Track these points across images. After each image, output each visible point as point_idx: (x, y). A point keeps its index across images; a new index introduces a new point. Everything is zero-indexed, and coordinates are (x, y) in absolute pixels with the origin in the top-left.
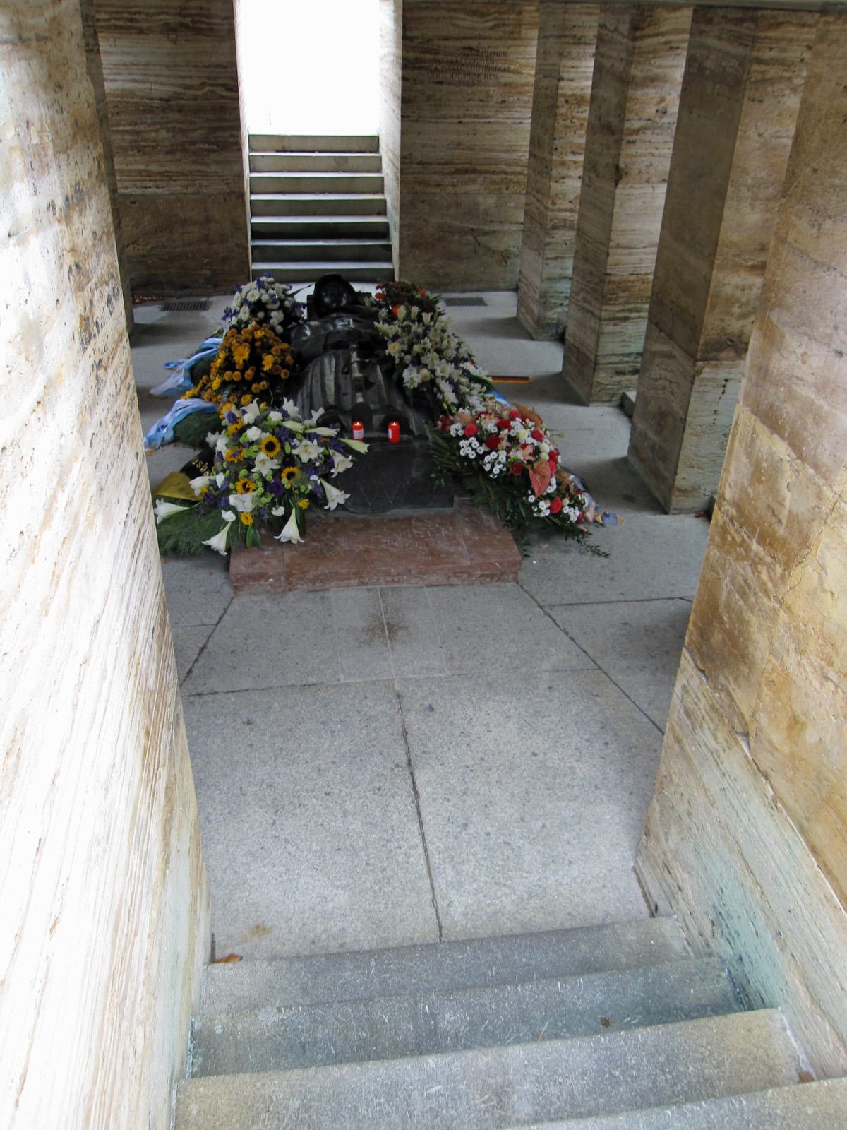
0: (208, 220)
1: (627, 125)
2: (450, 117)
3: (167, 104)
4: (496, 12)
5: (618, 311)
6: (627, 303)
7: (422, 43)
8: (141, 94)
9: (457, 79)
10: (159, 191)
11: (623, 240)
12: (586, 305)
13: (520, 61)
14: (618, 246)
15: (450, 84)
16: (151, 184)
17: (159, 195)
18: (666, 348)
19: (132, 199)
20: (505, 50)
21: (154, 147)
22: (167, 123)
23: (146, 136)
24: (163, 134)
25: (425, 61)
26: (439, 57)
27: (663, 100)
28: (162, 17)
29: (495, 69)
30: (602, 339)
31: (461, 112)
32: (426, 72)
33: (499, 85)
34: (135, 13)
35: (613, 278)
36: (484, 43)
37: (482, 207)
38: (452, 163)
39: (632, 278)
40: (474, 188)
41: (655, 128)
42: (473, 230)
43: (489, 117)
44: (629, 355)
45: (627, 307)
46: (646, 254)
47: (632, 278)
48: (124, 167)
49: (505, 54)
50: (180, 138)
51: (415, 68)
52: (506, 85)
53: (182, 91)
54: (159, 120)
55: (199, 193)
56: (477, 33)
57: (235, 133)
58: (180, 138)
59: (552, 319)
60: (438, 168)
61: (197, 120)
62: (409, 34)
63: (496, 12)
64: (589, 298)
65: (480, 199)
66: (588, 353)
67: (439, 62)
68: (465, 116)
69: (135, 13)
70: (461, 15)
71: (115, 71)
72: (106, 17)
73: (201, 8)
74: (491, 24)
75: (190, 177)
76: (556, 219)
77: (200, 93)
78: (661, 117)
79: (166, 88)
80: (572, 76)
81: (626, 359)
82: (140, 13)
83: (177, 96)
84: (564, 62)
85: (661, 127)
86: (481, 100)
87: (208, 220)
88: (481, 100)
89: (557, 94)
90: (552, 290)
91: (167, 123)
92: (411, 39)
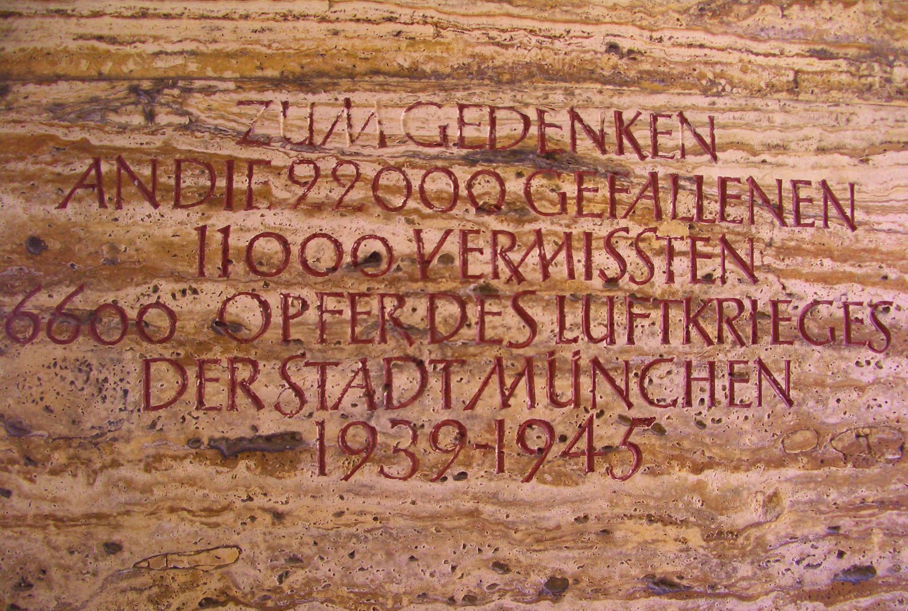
9: (430, 410)
20: (840, 171)
25: (118, 267)
32: (130, 356)
49: (838, 206)
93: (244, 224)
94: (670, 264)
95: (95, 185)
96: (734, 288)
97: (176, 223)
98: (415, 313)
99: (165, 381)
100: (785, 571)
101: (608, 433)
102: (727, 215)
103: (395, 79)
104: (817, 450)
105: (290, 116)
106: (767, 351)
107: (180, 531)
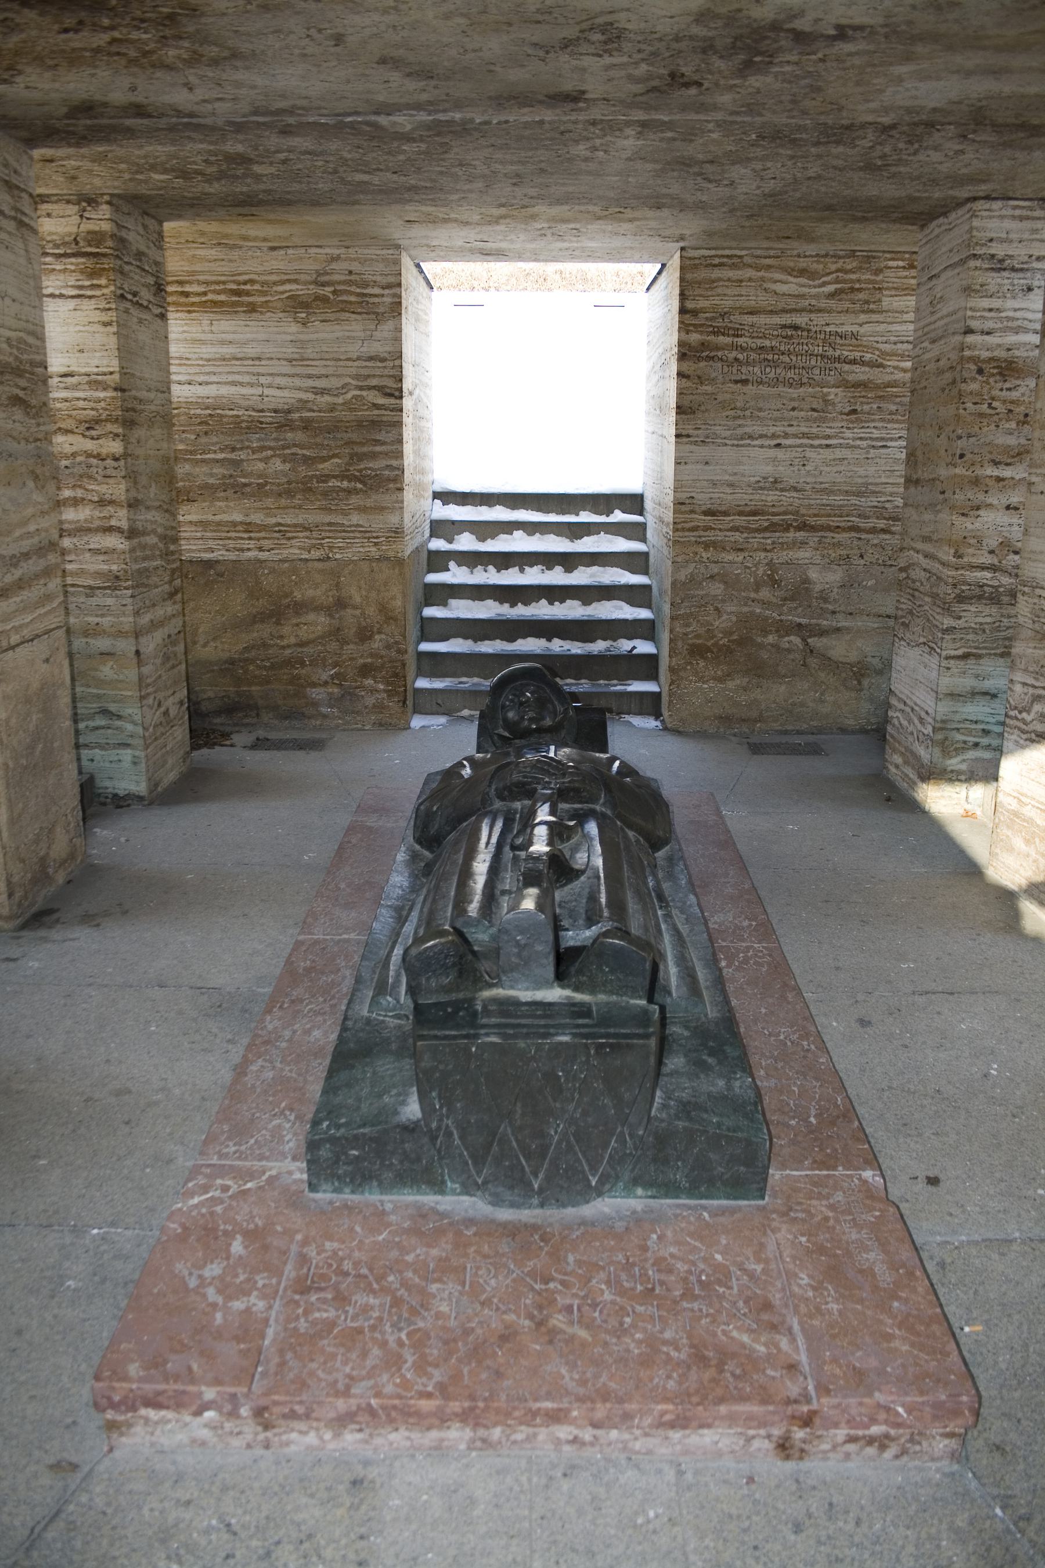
0: (341, 604)
2: (761, 436)
4: (837, 271)
7: (712, 319)
9: (772, 375)
16: (252, 544)
20: (855, 329)
22: (284, 448)
24: (277, 465)
26: (741, 341)
28: (287, 287)
32: (720, 365)
34: (245, 283)
36: (819, 319)
37: (818, 588)
40: (803, 555)
42: (800, 625)
43: (829, 437)
49: (854, 336)
50: (303, 471)
51: (699, 359)
52: (857, 385)
53: (310, 396)
54: (272, 444)
57: (394, 463)
58: (303, 471)
60: (740, 521)
62: (690, 305)
63: (837, 271)
65: (813, 574)
67: (743, 349)
68: (786, 435)
69: (245, 283)
70: (778, 276)
71: (207, 369)
72: (201, 289)
73: (350, 272)
75: (315, 534)
76: (965, 583)
77: (340, 400)
80: (990, 325)
82: (252, 282)
88: (814, 410)
90: (957, 717)
92: (695, 313)
93: (741, 341)
94: (137, 643)
95: (714, 333)
96: (831, 352)
97: (728, 340)
98: (770, 357)
99: (726, 369)
100: (839, 407)
101: (805, 380)
102: (831, 339)
104: (845, 384)
105: (749, 319)
106: (837, 365)
107: (728, 396)
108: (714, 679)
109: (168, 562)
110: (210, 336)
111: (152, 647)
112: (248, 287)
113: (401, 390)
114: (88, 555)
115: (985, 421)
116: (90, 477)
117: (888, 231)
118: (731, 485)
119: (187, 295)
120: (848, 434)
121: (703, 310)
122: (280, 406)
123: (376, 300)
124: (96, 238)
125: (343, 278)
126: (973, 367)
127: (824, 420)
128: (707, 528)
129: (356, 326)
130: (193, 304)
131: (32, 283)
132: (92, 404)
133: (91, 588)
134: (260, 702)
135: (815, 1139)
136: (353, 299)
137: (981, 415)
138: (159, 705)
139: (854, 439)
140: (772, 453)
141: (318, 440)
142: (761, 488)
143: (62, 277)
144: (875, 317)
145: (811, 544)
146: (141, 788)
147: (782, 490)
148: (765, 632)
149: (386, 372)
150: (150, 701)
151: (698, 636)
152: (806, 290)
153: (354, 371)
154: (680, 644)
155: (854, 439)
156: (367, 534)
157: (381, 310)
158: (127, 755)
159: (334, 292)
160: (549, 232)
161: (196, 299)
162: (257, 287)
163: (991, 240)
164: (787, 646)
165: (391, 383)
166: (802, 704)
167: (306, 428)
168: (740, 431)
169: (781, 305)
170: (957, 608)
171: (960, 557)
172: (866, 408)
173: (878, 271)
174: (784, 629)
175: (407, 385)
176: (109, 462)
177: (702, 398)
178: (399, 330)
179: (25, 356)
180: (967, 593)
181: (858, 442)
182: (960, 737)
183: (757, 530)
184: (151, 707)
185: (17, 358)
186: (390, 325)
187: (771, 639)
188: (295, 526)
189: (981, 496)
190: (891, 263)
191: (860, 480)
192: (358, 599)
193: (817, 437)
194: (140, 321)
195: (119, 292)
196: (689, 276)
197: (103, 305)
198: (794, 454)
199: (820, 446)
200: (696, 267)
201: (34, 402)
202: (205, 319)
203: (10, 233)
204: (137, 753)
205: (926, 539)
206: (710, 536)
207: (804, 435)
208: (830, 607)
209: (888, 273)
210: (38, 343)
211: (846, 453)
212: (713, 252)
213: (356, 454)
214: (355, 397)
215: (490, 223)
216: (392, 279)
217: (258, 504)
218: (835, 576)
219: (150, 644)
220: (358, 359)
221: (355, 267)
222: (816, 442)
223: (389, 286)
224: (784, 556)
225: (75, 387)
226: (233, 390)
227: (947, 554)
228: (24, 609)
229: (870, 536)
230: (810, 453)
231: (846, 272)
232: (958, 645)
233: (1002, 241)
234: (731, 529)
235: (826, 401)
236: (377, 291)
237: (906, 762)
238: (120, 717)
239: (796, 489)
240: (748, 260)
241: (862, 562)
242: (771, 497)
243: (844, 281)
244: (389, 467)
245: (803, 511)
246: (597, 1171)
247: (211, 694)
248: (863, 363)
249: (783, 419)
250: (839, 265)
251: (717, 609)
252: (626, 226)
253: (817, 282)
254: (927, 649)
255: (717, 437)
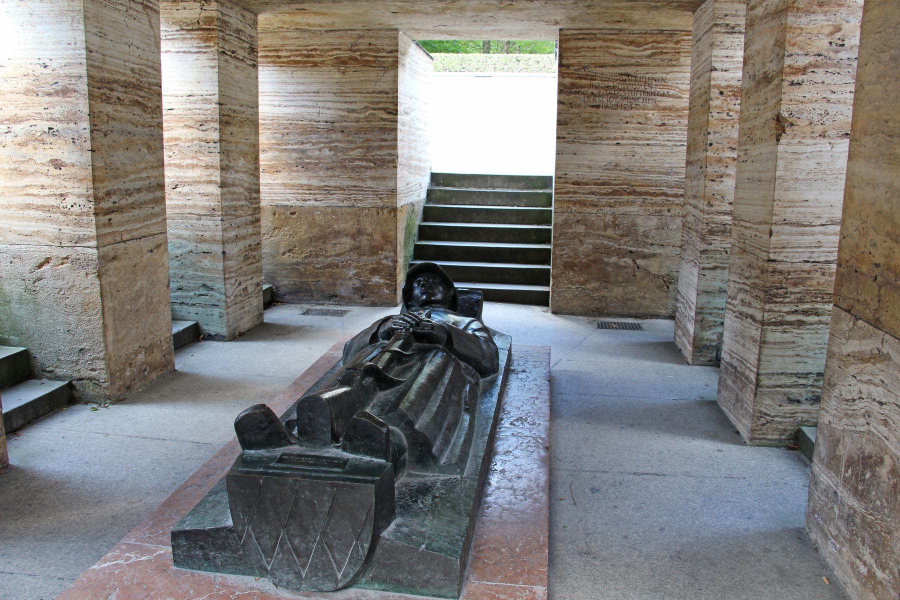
0: (360, 232)
1: (788, 61)
2: (608, 139)
3: (331, 127)
4: (653, 42)
5: (788, 313)
6: (801, 301)
7: (578, 70)
8: (310, 117)
9: (614, 103)
10: (317, 204)
11: (791, 215)
12: (745, 310)
13: (680, 86)
14: (785, 222)
15: (607, 107)
16: (311, 197)
17: (316, 208)
18: (869, 346)
19: (292, 210)
20: (664, 76)
21: (316, 164)
22: (330, 142)
23: (309, 154)
24: (327, 152)
25: (582, 87)
26: (595, 82)
27: (838, 29)
28: (335, 52)
29: (654, 94)
30: (766, 351)
31: (618, 135)
32: (582, 96)
33: (657, 108)
34: (312, 50)
35: (779, 267)
36: (641, 71)
37: (642, 229)
38: (609, 184)
39: (807, 267)
40: (634, 209)
41: (828, 66)
42: (631, 252)
43: (648, 139)
44: (806, 375)
45: (802, 307)
46: (824, 234)
47: (807, 267)
48: (289, 182)
49: (663, 80)
50: (341, 156)
51: (570, 93)
52: (665, 109)
53: (346, 114)
54: (324, 140)
55: (354, 206)
56: (633, 61)
57: (392, 152)
58: (341, 156)
59: (712, 341)
60: (595, 188)
61: (357, 140)
62: (565, 62)
63: (653, 42)
64: (748, 298)
65: (639, 221)
66: (747, 372)
67: (596, 87)
68: (623, 138)
69: (312, 50)
70: (617, 45)
71: (290, 98)
72: (288, 54)
73: (370, 44)
74: (649, 52)
75: (346, 192)
76: (713, 223)
77: (362, 116)
78: (837, 52)
79: (332, 112)
80: (725, 66)
81: (802, 381)
82: (315, 50)
83: (343, 119)
84: (715, 52)
85: (838, 64)
86: (640, 123)
87: (360, 232)
88: (640, 123)
89: (710, 86)
90: (710, 306)
91: (330, 142)
92: (568, 66)
93: (595, 82)
95: (579, 78)
96: (649, 90)
97: (588, 82)
99: (586, 99)
100: (654, 122)
103: (659, 198)
105: (599, 70)
107: (587, 115)
108: (579, 282)
109: (252, 203)
110: (292, 80)
111: (235, 250)
112: (313, 53)
113: (397, 110)
114: (198, 196)
115: (725, 124)
116: (201, 152)
117: (676, 16)
118: (589, 167)
119: (280, 57)
120: (660, 137)
121: (573, 65)
122: (329, 119)
123: (382, 59)
124: (209, 20)
125: (365, 47)
126: (717, 91)
127: (646, 129)
128: (575, 193)
129: (372, 74)
130: (283, 62)
131: (153, 39)
132: (203, 112)
133: (199, 215)
134: (313, 288)
135: (513, 562)
136: (371, 59)
137: (722, 120)
138: (240, 284)
139: (664, 141)
140: (614, 148)
141: (350, 138)
142: (608, 169)
143: (190, 42)
144: (676, 69)
145: (638, 203)
146: (224, 331)
147: (621, 170)
148: (609, 254)
149: (389, 100)
150: (233, 281)
151: (570, 257)
152: (634, 53)
153: (371, 100)
154: (558, 261)
155: (664, 141)
156: (376, 193)
157: (386, 65)
158: (216, 311)
159: (361, 55)
160: (477, 19)
161: (285, 60)
162: (318, 52)
163: (726, 15)
164: (623, 264)
165: (391, 106)
166: (633, 300)
167: (342, 131)
168: (595, 136)
169: (619, 62)
170: (709, 238)
171: (712, 206)
172: (671, 122)
173: (678, 42)
174: (621, 254)
175: (400, 108)
176: (212, 144)
177: (572, 116)
178: (396, 76)
179: (145, 79)
180: (715, 229)
181: (666, 143)
182: (710, 318)
183: (605, 194)
184: (233, 285)
185: (138, 79)
186: (391, 73)
187: (613, 259)
188: (336, 187)
189: (723, 170)
190: (685, 38)
191: (667, 165)
192: (370, 230)
193: (641, 139)
194: (237, 67)
195: (221, 50)
196: (564, 45)
197: (211, 57)
198: (627, 149)
199: (643, 145)
200: (568, 40)
201: (150, 105)
202: (289, 70)
203: (137, 11)
204: (222, 311)
205: (695, 197)
206: (577, 197)
207: (634, 138)
208: (650, 241)
209: (683, 43)
210: (156, 73)
211: (658, 149)
212: (578, 32)
213: (371, 147)
214: (371, 114)
215: (440, 13)
216: (392, 48)
217: (315, 174)
218: (653, 222)
219: (232, 249)
220: (373, 92)
221: (373, 41)
222: (641, 142)
223: (391, 52)
224: (623, 209)
225: (195, 103)
226: (303, 109)
227: (702, 204)
228: (136, 220)
229: (674, 199)
230: (637, 149)
231: (658, 43)
232: (710, 261)
233: (734, 16)
234: (589, 193)
235: (646, 118)
236: (385, 54)
237: (683, 334)
238: (212, 289)
239: (628, 170)
240: (599, 36)
241: (669, 214)
242: (614, 174)
243: (657, 48)
244: (389, 154)
245: (633, 183)
246: (341, 568)
247: (286, 282)
248: (669, 96)
249: (621, 128)
250: (654, 39)
251: (581, 241)
252: (519, 14)
253: (641, 49)
254: (693, 264)
255: (581, 138)
